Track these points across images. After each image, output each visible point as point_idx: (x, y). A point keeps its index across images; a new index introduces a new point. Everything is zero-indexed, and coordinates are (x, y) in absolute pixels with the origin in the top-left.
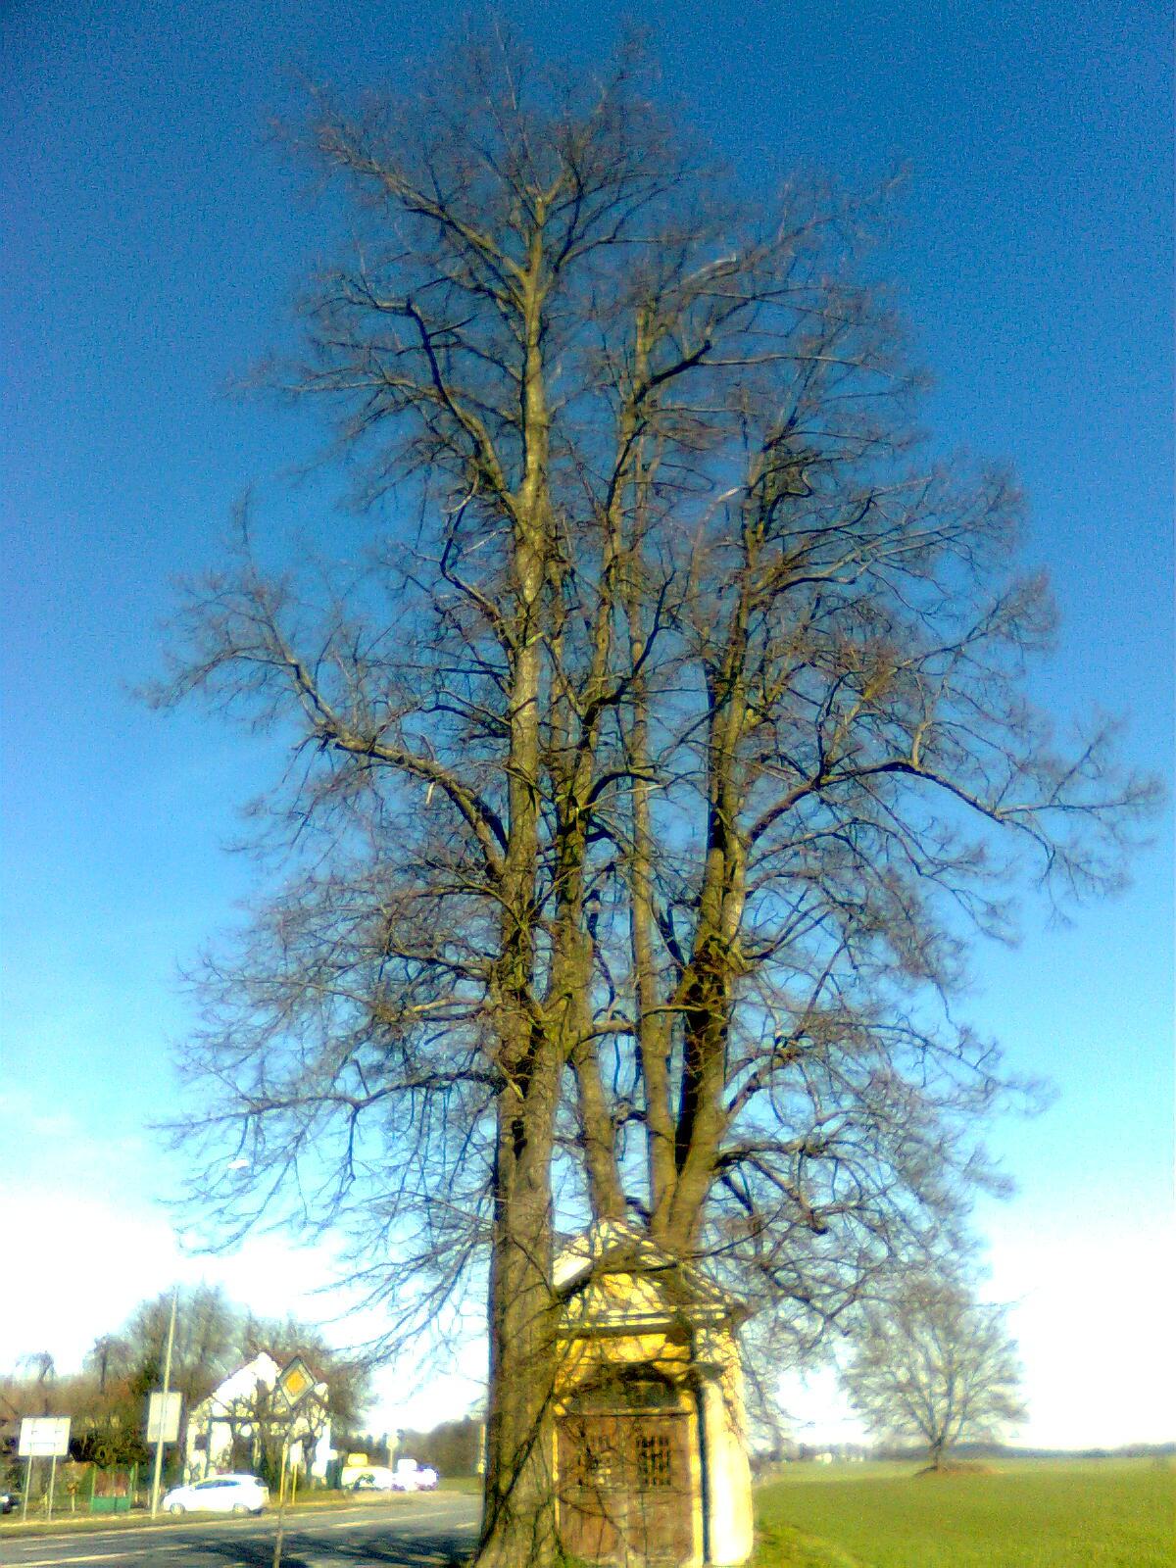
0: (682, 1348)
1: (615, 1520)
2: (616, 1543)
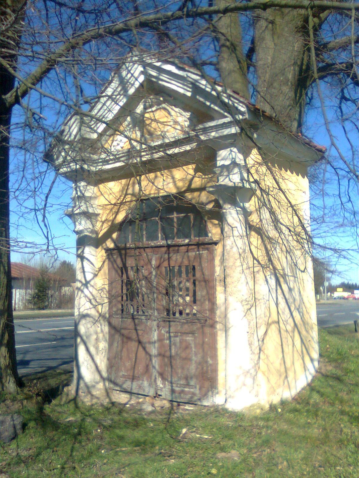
1: (147, 345)
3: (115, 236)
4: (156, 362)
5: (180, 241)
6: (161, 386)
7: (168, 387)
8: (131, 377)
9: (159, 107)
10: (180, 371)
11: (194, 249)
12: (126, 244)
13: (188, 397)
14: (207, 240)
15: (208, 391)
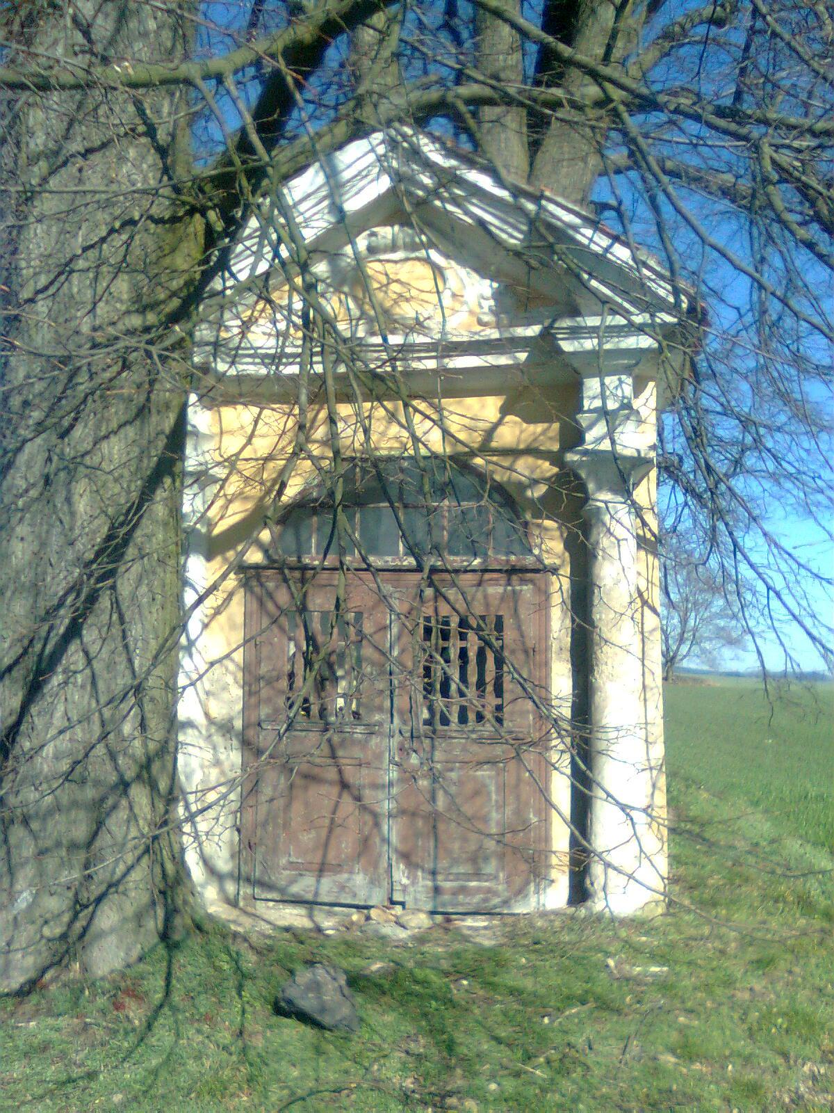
0: (539, 428)
1: (367, 793)
2: (365, 844)
3: (265, 535)
4: (393, 830)
5: (456, 561)
6: (405, 881)
7: (424, 882)
8: (316, 867)
9: (413, 255)
10: (456, 846)
11: (497, 580)
12: (299, 558)
13: (477, 899)
14: (529, 561)
15: (527, 883)
